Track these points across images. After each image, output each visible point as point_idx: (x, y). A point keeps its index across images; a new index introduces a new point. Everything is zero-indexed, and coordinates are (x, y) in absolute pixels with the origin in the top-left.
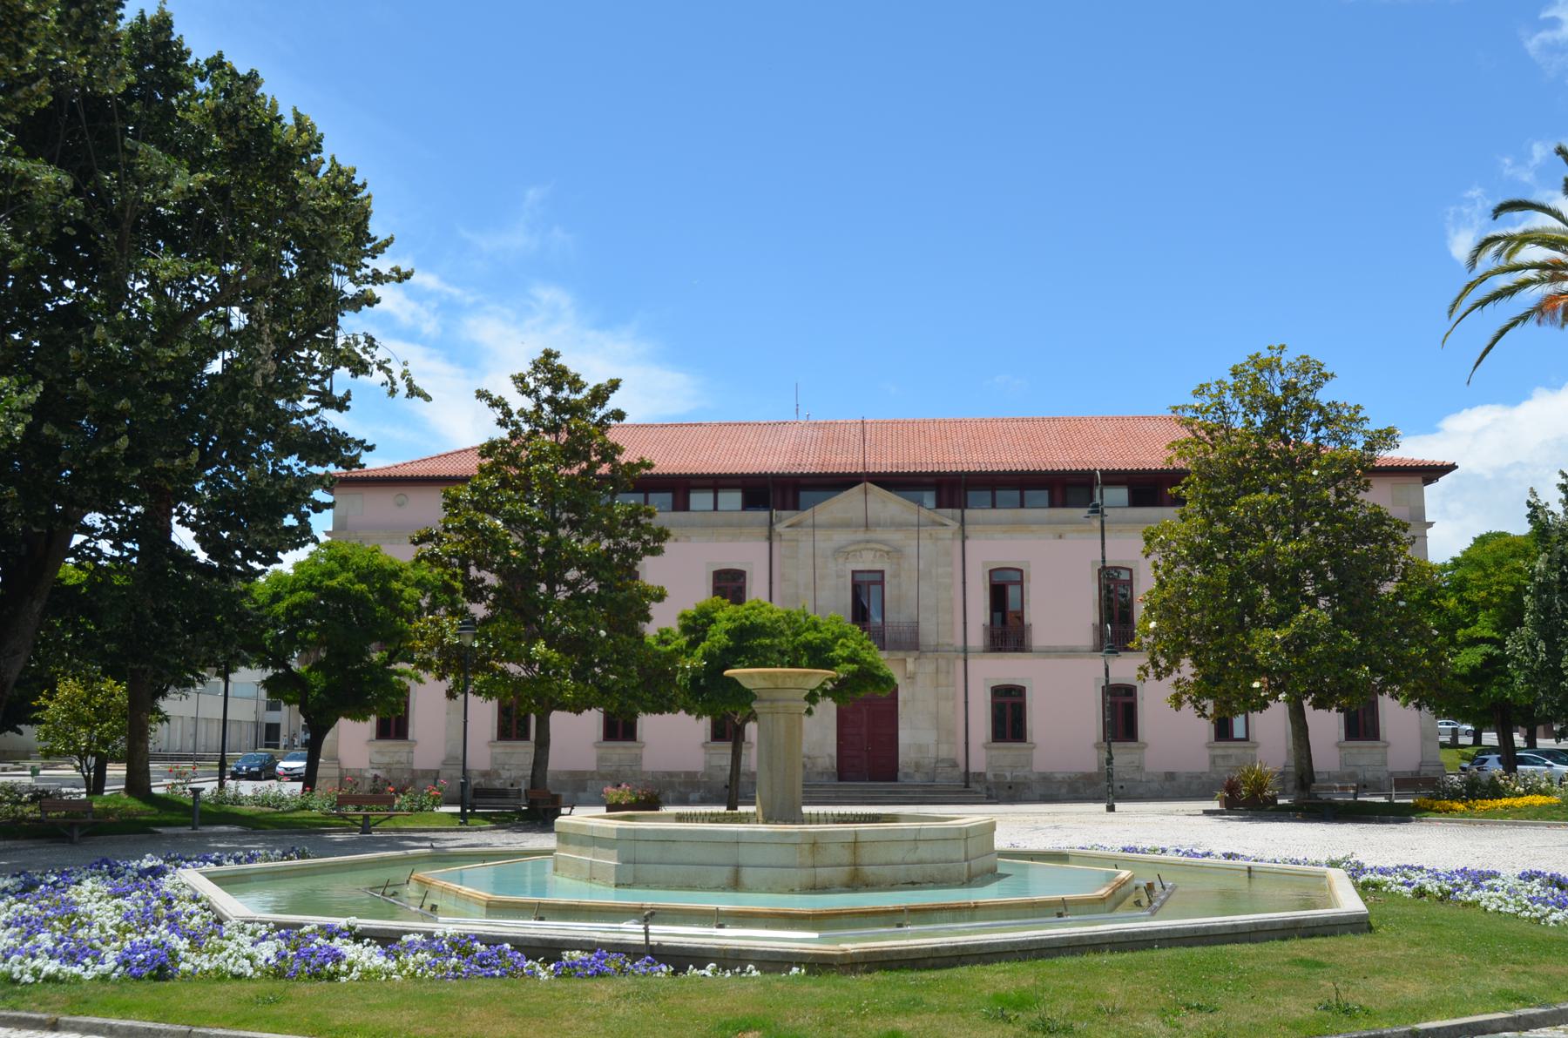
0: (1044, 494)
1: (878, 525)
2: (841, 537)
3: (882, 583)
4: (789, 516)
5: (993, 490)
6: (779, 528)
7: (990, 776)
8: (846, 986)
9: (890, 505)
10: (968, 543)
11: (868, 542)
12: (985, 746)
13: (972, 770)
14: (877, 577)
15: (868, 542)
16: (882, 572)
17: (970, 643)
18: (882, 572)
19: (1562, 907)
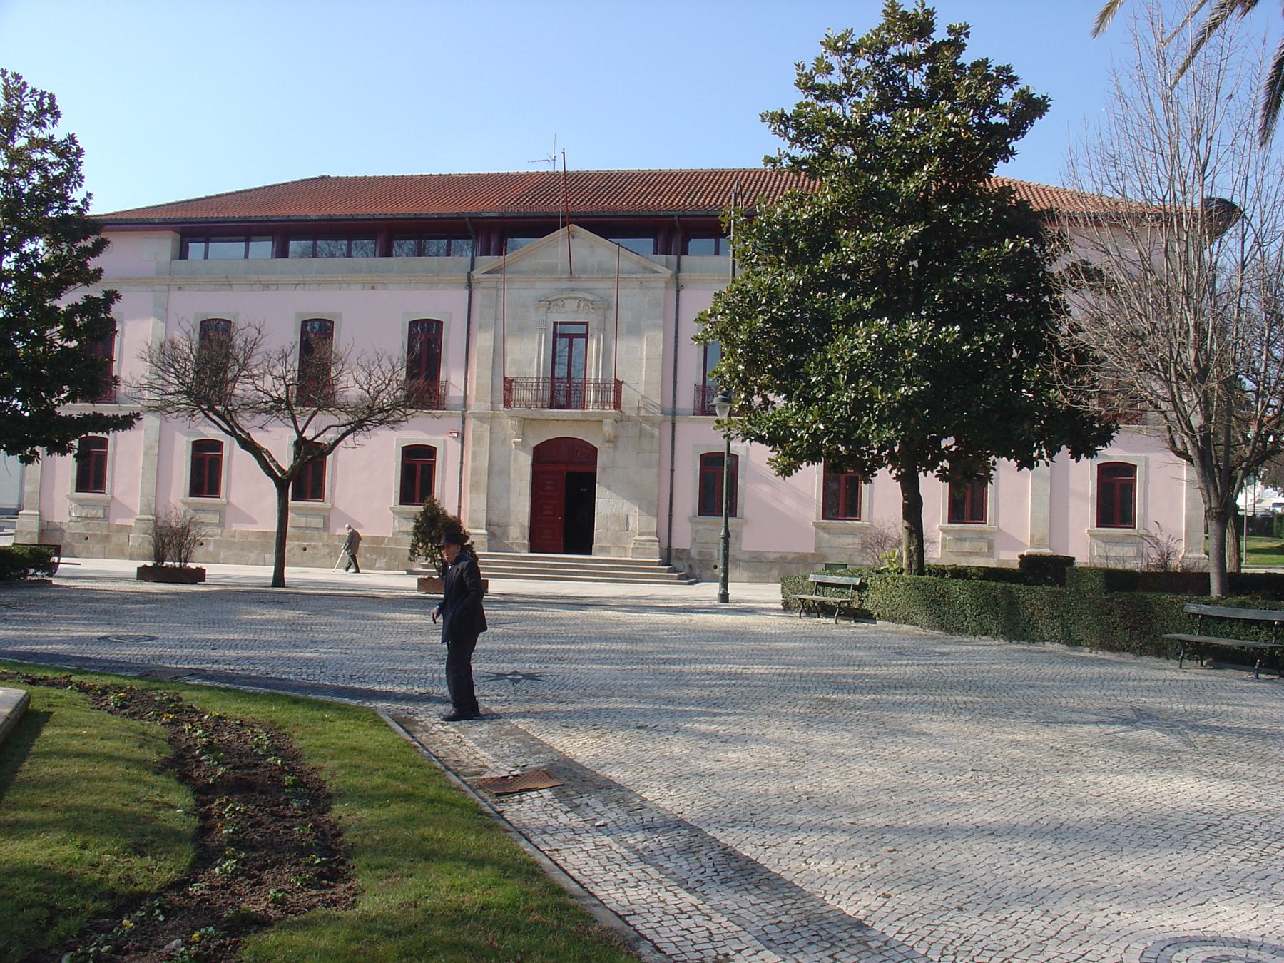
0: (370, 244)
1: (585, 271)
2: (543, 288)
3: (585, 336)
4: (487, 262)
5: (349, 240)
6: (476, 275)
7: (694, 554)
8: (138, 800)
9: (591, 250)
10: (682, 292)
11: (573, 290)
12: (691, 520)
13: (675, 545)
14: (582, 330)
15: (573, 290)
16: (587, 324)
17: (680, 405)
18: (587, 324)
19: (4, 897)
